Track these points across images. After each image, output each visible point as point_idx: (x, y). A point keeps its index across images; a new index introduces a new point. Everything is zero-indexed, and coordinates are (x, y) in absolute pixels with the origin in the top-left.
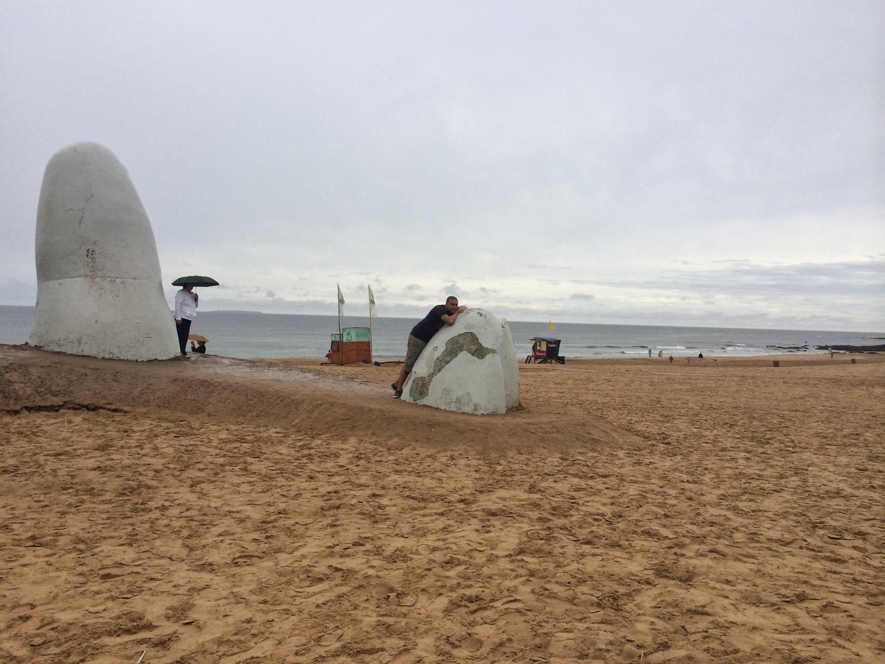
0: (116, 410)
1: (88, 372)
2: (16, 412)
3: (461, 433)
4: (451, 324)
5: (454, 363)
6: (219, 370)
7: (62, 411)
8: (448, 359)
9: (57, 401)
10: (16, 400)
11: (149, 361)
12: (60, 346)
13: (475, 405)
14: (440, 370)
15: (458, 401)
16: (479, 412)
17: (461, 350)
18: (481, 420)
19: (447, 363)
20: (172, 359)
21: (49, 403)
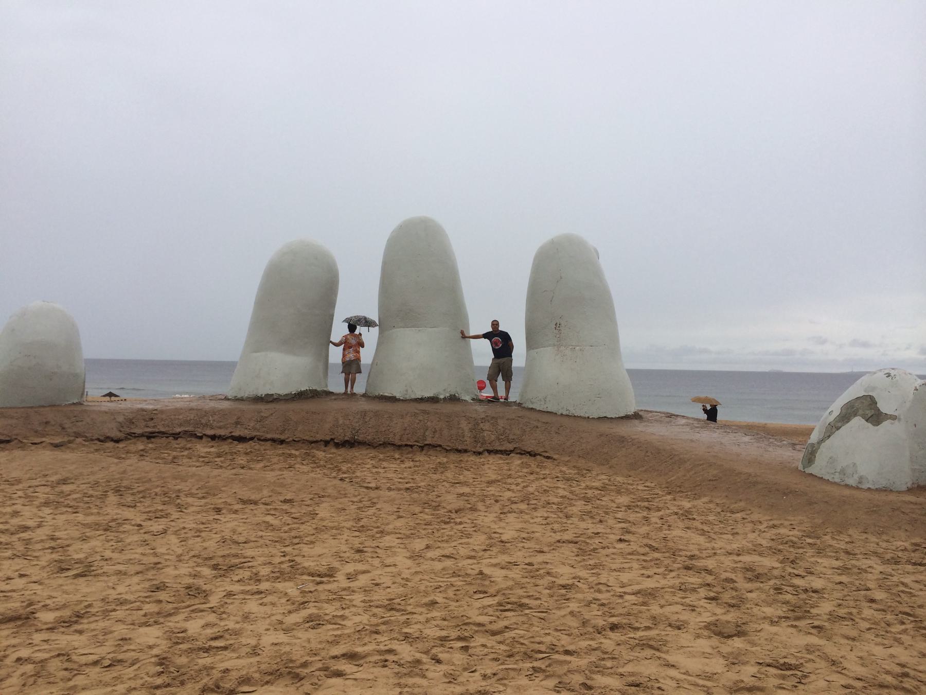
0: (548, 458)
1: (539, 425)
2: (480, 453)
3: (810, 503)
4: (365, 318)
5: (845, 429)
6: (651, 429)
7: (512, 455)
8: (840, 424)
9: (510, 447)
10: (482, 444)
11: (599, 418)
12: (532, 403)
13: (861, 478)
14: (829, 436)
15: (843, 472)
16: (865, 486)
17: (855, 415)
18: (867, 494)
19: (838, 428)
20: (622, 418)
21: (503, 448)
